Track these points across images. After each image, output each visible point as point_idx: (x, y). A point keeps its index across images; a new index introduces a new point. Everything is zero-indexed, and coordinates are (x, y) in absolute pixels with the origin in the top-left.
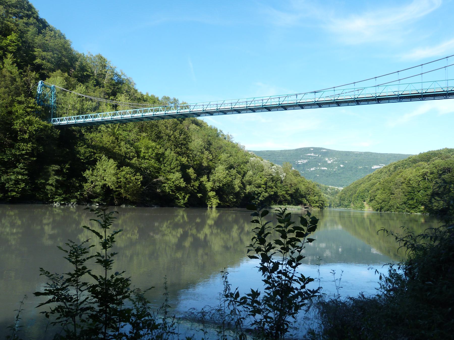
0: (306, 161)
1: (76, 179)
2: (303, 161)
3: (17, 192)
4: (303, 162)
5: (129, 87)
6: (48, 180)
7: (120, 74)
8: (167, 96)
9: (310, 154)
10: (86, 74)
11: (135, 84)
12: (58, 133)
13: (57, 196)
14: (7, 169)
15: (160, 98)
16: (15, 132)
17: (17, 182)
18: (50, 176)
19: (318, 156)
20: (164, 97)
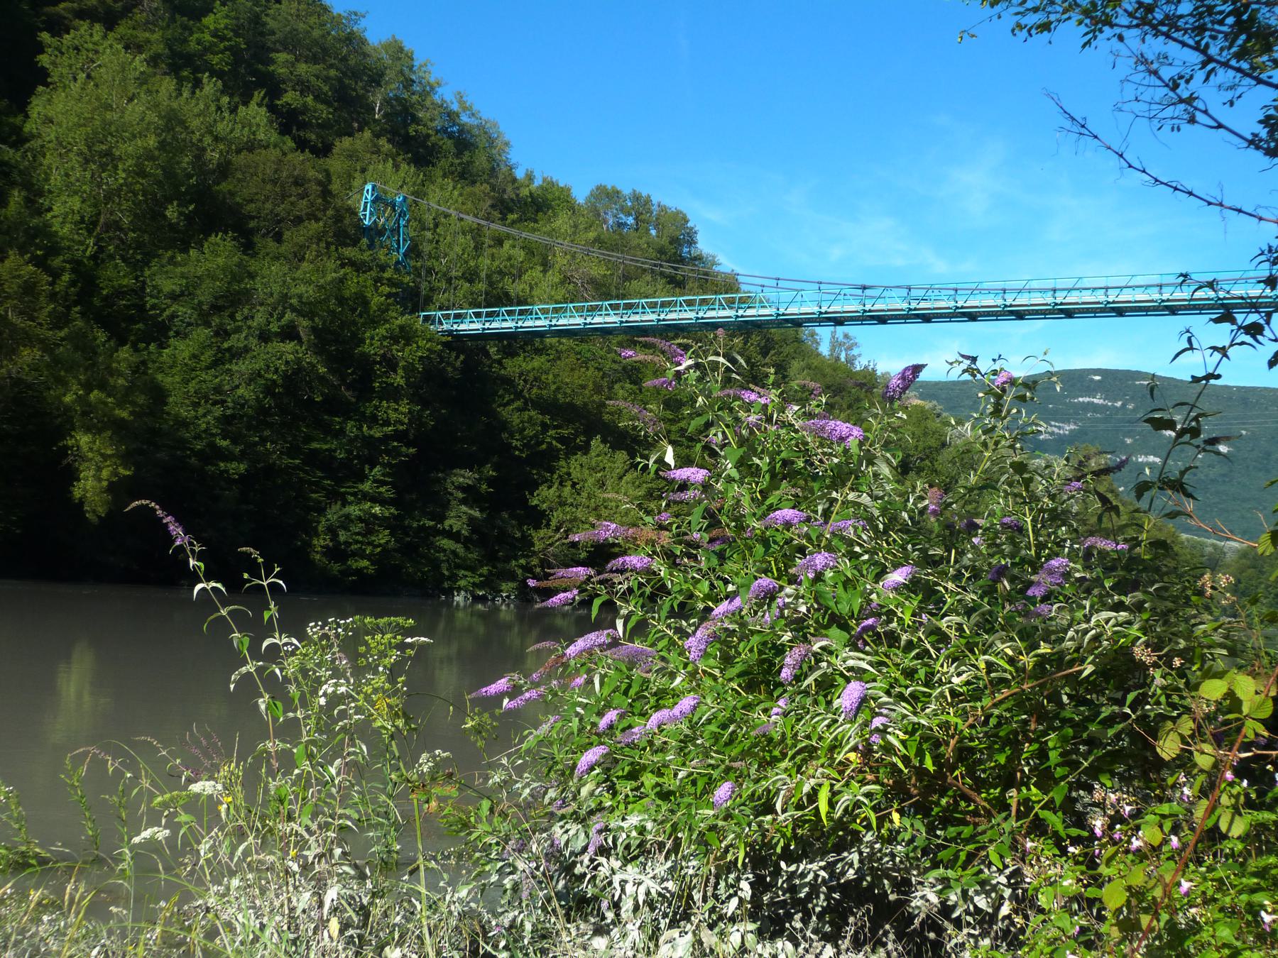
0: (1072, 427)
1: (512, 516)
2: (1059, 428)
3: (369, 558)
4: (1056, 430)
5: (491, 159)
6: (442, 519)
7: (455, 107)
8: (609, 187)
9: (1087, 400)
10: (416, 131)
11: (507, 144)
12: (458, 364)
13: (462, 572)
14: (339, 482)
15: (580, 195)
16: (365, 365)
17: (370, 523)
18: (446, 506)
19: (1124, 405)
20: (598, 188)
